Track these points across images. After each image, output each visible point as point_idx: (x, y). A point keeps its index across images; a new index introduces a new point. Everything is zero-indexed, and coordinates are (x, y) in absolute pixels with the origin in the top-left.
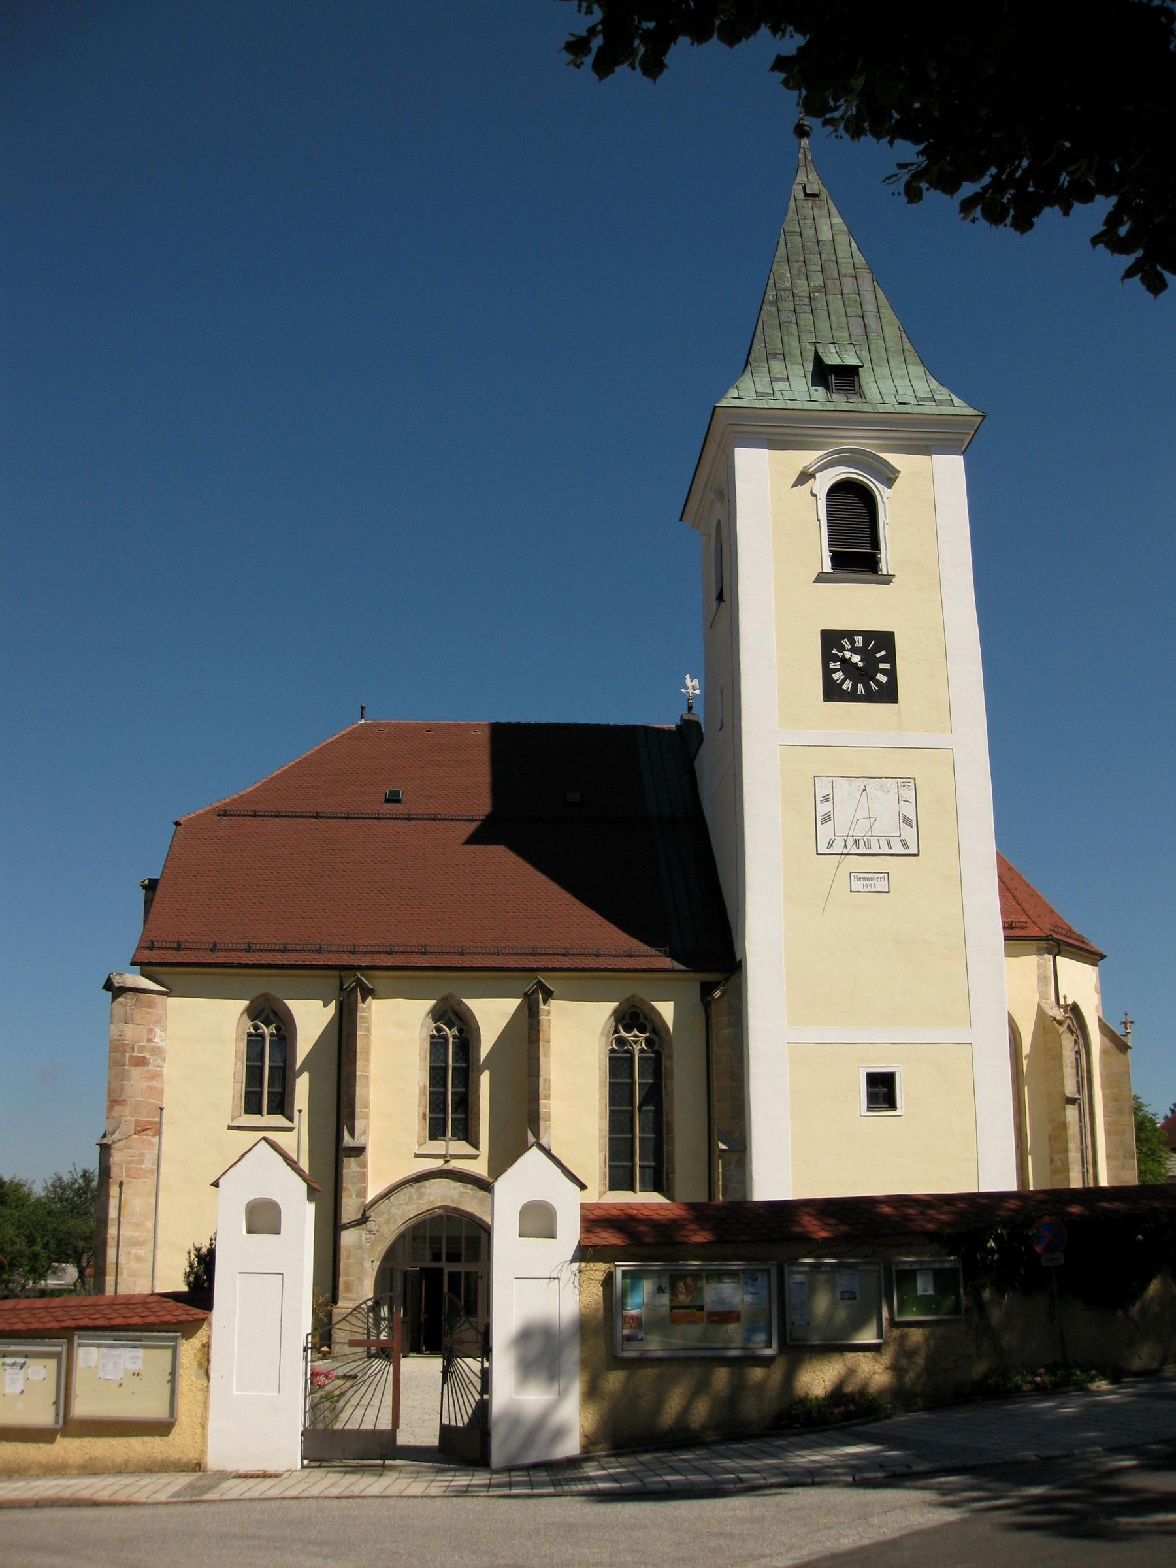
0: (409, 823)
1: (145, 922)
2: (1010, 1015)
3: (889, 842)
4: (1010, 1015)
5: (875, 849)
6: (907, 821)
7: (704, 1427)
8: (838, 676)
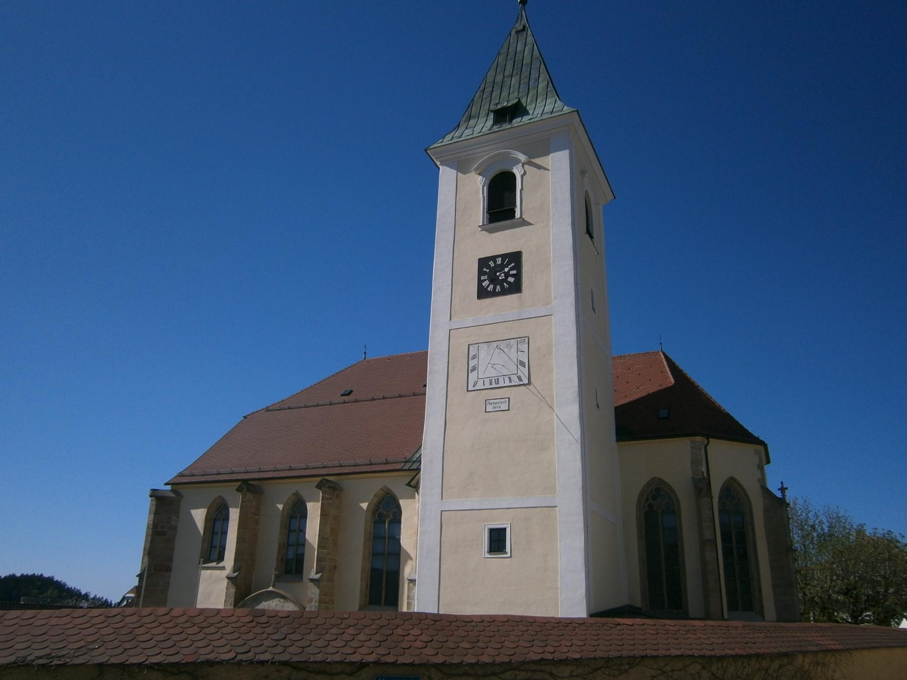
0: (357, 404)
1: (268, 410)
2: (530, 224)
3: (510, 379)
4: (530, 224)
5: (501, 384)
6: (522, 364)
7: (601, 614)
8: (485, 284)
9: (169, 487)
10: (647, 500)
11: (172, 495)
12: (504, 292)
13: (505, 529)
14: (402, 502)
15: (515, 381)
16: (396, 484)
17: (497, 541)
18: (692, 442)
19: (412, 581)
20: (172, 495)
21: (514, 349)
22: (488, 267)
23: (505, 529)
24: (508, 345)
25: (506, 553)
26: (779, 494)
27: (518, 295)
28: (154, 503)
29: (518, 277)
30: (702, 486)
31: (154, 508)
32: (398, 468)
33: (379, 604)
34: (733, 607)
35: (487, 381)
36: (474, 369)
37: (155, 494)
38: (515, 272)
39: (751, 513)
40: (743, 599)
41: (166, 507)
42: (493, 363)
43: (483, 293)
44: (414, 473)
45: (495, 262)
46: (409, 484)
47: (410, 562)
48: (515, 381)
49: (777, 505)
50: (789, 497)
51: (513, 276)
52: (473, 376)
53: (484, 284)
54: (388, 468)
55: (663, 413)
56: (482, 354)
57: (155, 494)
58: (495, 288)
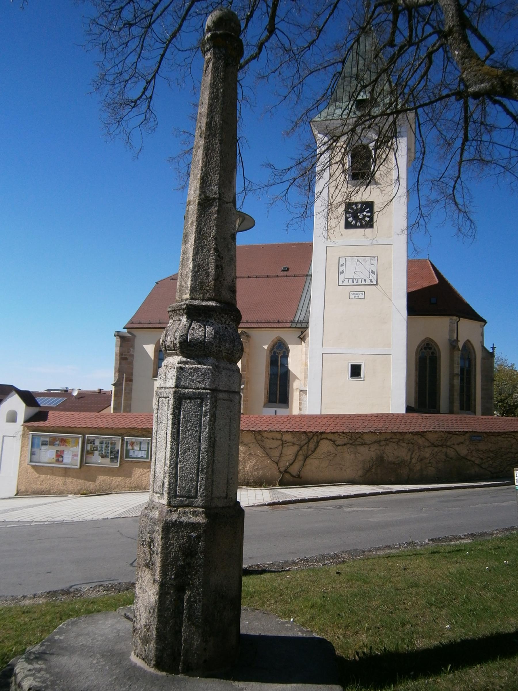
3: (365, 280)
5: (360, 283)
6: (373, 272)
8: (350, 219)
9: (126, 330)
10: (421, 349)
11: (129, 335)
12: (362, 227)
13: (361, 365)
14: (289, 346)
15: (368, 282)
16: (286, 335)
17: (356, 371)
18: (451, 319)
19: (303, 391)
20: (129, 335)
21: (368, 263)
22: (352, 209)
23: (361, 365)
24: (364, 260)
25: (361, 378)
26: (491, 350)
27: (371, 229)
28: (119, 340)
29: (371, 218)
30: (453, 344)
31: (119, 343)
32: (288, 326)
33: (276, 402)
34: (462, 408)
35: (351, 281)
36: (342, 272)
37: (118, 334)
38: (369, 214)
39: (475, 359)
40: (467, 405)
41: (126, 343)
42: (352, 270)
43: (348, 225)
44: (303, 330)
45: (356, 206)
46: (299, 337)
47: (297, 381)
48: (368, 282)
49: (489, 356)
50: (497, 353)
51: (368, 217)
52: (342, 277)
53: (349, 220)
54: (279, 325)
55: (433, 300)
56: (348, 263)
57: (118, 334)
58: (356, 223)
